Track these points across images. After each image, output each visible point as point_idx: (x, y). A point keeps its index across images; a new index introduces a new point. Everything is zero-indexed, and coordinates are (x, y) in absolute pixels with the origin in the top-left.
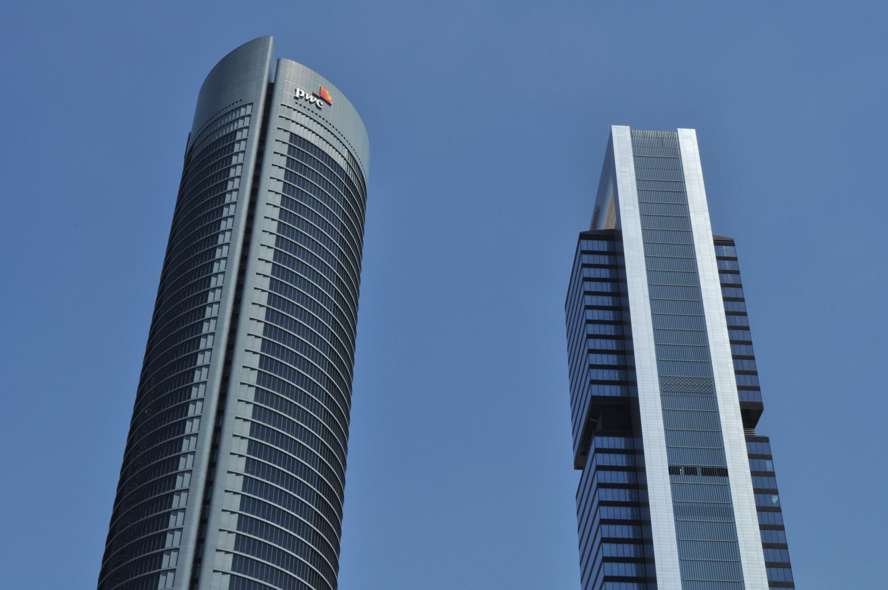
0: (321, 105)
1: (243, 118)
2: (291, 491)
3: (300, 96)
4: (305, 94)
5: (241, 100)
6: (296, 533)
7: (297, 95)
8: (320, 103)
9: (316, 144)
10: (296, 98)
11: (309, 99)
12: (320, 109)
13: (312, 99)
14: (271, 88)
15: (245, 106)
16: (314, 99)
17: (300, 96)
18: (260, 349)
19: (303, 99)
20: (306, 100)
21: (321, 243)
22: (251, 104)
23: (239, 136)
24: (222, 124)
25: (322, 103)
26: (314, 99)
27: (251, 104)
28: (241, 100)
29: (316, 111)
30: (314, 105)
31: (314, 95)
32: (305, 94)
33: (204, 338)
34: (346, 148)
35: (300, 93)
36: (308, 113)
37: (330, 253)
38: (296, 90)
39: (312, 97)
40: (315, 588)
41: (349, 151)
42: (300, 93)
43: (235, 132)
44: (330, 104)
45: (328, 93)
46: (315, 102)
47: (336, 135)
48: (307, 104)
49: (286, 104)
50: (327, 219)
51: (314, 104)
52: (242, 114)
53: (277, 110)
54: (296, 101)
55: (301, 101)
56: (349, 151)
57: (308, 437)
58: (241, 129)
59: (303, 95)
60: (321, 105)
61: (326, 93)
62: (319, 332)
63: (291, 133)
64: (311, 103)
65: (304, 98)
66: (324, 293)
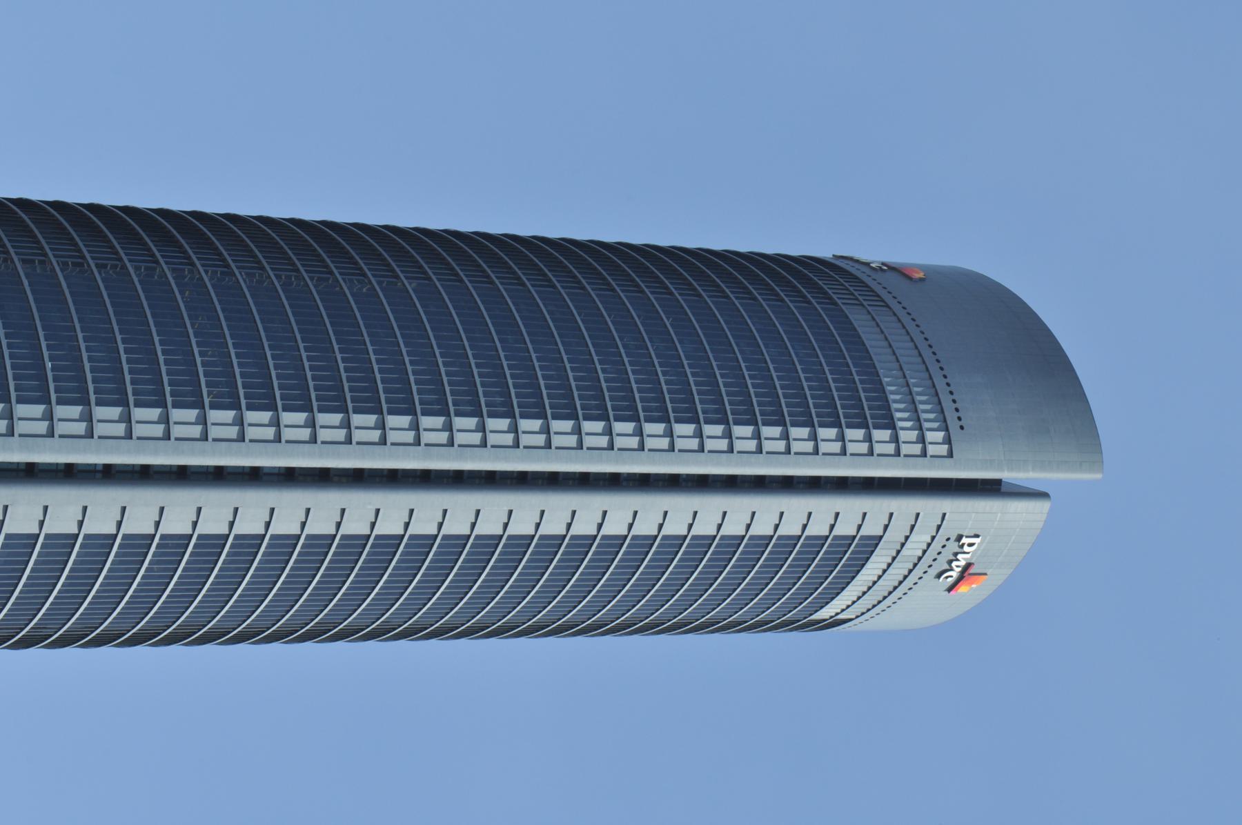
0: (947, 577)
1: (922, 440)
2: (337, 548)
3: (963, 544)
4: (968, 553)
5: (962, 428)
6: (223, 563)
7: (964, 540)
8: (951, 576)
9: (859, 577)
10: (959, 538)
11: (958, 560)
12: (939, 576)
13: (962, 560)
14: (990, 488)
15: (948, 441)
16: (957, 566)
17: (963, 544)
18: (9, 532)
19: (958, 550)
20: (956, 554)
21: (768, 554)
22: (950, 454)
23: (881, 435)
24: (918, 398)
25: (950, 579)
26: (957, 566)
27: (950, 454)
28: (962, 428)
29: (933, 572)
30: (946, 567)
31: (968, 566)
32: (968, 553)
33: (891, 436)
34: (857, 617)
35: (971, 545)
36: (931, 553)
37: (750, 572)
38: (977, 536)
39: (963, 563)
40: (6, 615)
41: (851, 620)
42: (971, 545)
43: (891, 425)
44: (950, 589)
45: (974, 586)
46: (952, 569)
47: (892, 595)
48: (947, 554)
49: (945, 522)
50: (820, 561)
51: (948, 567)
52: (930, 436)
53: (930, 507)
54: (953, 538)
55: (953, 546)
56: (851, 620)
57: (407, 568)
58: (895, 439)
59: (966, 549)
60: (947, 577)
61: (973, 584)
62: (656, 553)
63: (881, 537)
64: (950, 562)
65: (960, 550)
66: (701, 562)
